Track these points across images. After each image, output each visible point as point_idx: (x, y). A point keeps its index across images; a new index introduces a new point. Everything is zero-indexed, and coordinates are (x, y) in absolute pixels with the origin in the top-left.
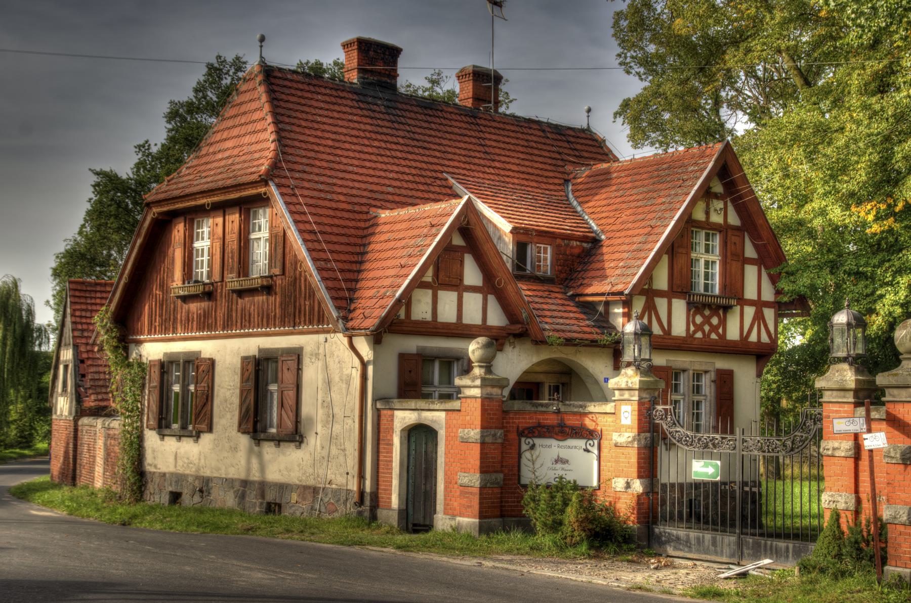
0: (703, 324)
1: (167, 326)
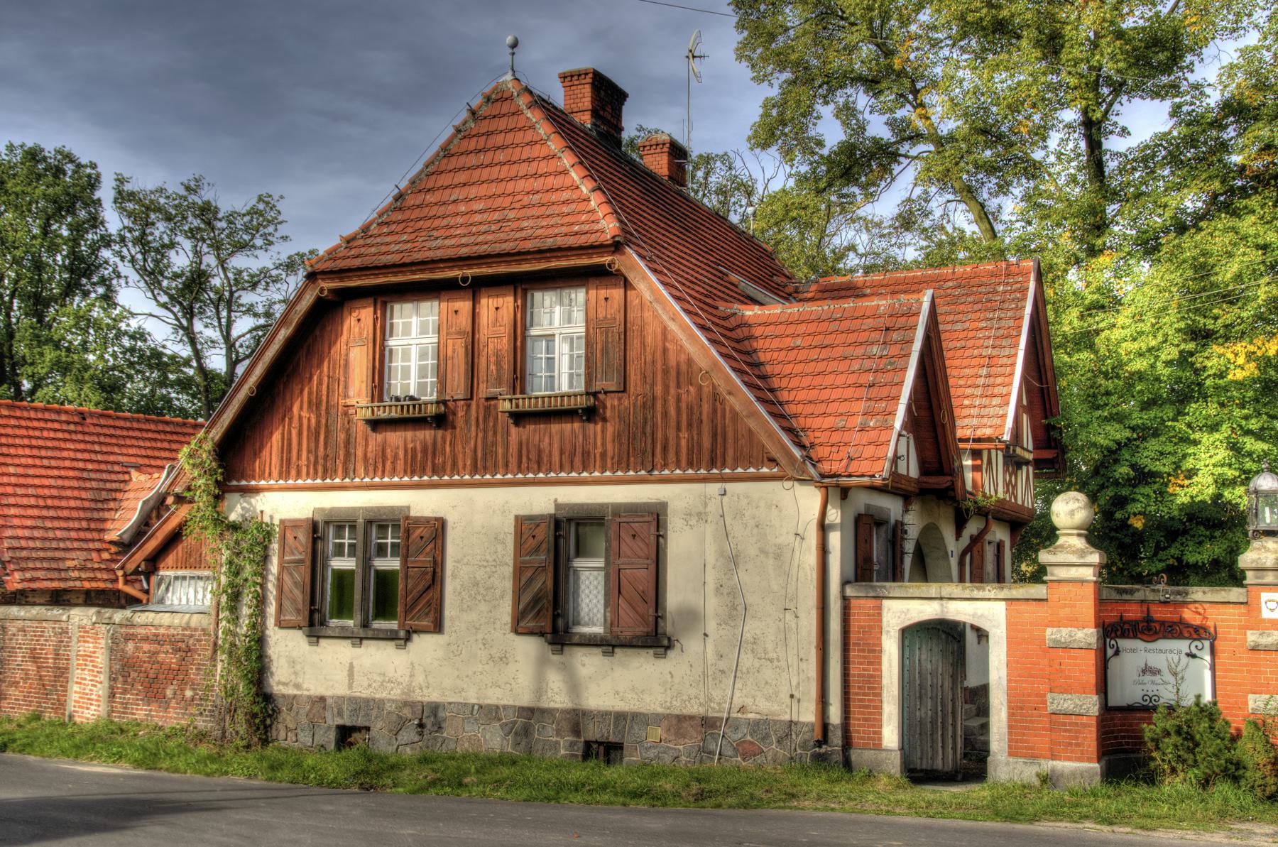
1: (329, 463)
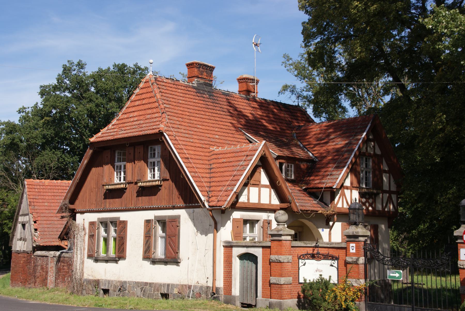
0: (366, 202)
